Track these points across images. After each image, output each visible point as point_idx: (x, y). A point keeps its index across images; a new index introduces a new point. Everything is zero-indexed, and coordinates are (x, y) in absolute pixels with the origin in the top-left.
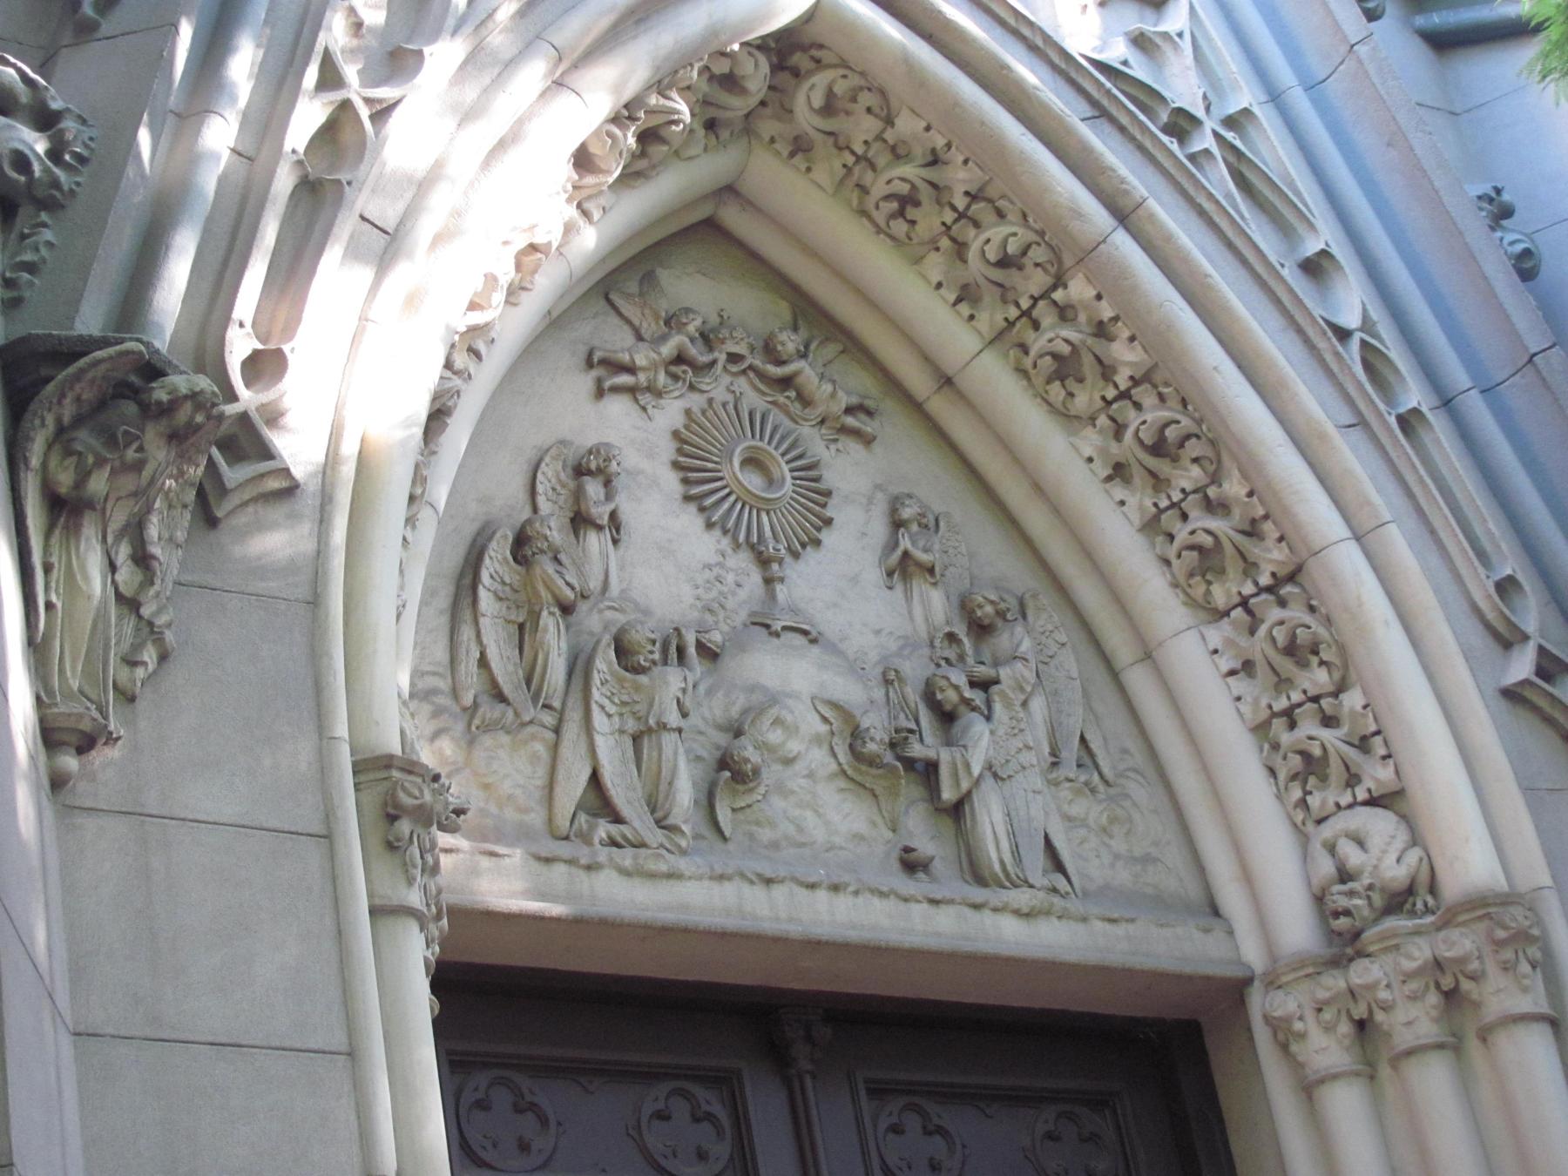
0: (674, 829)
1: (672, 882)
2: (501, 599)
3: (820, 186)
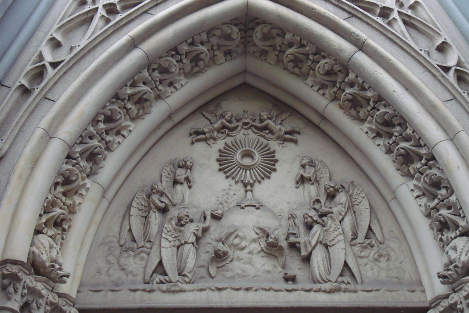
0: (185, 275)
1: (181, 293)
2: (140, 210)
3: (271, 64)
